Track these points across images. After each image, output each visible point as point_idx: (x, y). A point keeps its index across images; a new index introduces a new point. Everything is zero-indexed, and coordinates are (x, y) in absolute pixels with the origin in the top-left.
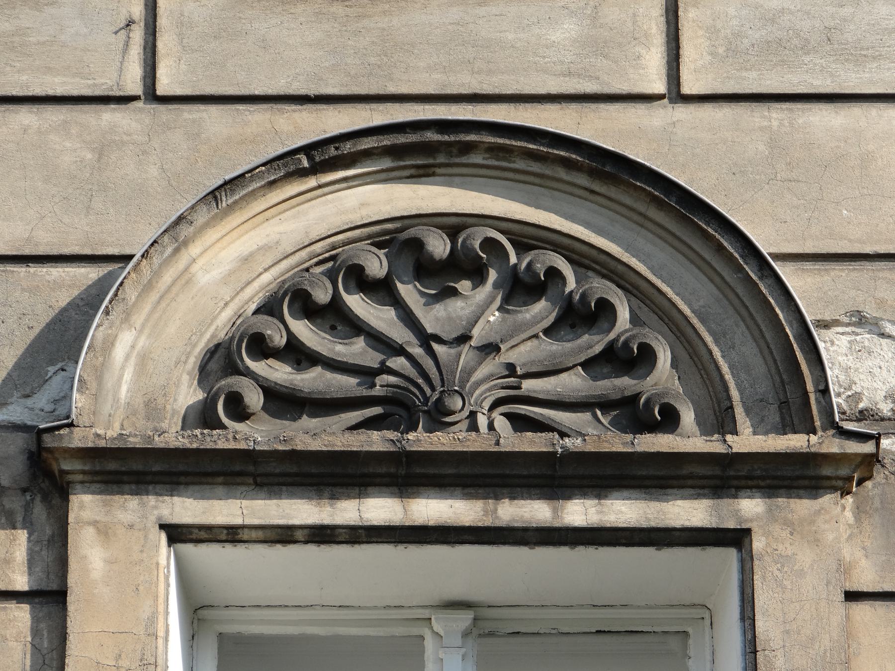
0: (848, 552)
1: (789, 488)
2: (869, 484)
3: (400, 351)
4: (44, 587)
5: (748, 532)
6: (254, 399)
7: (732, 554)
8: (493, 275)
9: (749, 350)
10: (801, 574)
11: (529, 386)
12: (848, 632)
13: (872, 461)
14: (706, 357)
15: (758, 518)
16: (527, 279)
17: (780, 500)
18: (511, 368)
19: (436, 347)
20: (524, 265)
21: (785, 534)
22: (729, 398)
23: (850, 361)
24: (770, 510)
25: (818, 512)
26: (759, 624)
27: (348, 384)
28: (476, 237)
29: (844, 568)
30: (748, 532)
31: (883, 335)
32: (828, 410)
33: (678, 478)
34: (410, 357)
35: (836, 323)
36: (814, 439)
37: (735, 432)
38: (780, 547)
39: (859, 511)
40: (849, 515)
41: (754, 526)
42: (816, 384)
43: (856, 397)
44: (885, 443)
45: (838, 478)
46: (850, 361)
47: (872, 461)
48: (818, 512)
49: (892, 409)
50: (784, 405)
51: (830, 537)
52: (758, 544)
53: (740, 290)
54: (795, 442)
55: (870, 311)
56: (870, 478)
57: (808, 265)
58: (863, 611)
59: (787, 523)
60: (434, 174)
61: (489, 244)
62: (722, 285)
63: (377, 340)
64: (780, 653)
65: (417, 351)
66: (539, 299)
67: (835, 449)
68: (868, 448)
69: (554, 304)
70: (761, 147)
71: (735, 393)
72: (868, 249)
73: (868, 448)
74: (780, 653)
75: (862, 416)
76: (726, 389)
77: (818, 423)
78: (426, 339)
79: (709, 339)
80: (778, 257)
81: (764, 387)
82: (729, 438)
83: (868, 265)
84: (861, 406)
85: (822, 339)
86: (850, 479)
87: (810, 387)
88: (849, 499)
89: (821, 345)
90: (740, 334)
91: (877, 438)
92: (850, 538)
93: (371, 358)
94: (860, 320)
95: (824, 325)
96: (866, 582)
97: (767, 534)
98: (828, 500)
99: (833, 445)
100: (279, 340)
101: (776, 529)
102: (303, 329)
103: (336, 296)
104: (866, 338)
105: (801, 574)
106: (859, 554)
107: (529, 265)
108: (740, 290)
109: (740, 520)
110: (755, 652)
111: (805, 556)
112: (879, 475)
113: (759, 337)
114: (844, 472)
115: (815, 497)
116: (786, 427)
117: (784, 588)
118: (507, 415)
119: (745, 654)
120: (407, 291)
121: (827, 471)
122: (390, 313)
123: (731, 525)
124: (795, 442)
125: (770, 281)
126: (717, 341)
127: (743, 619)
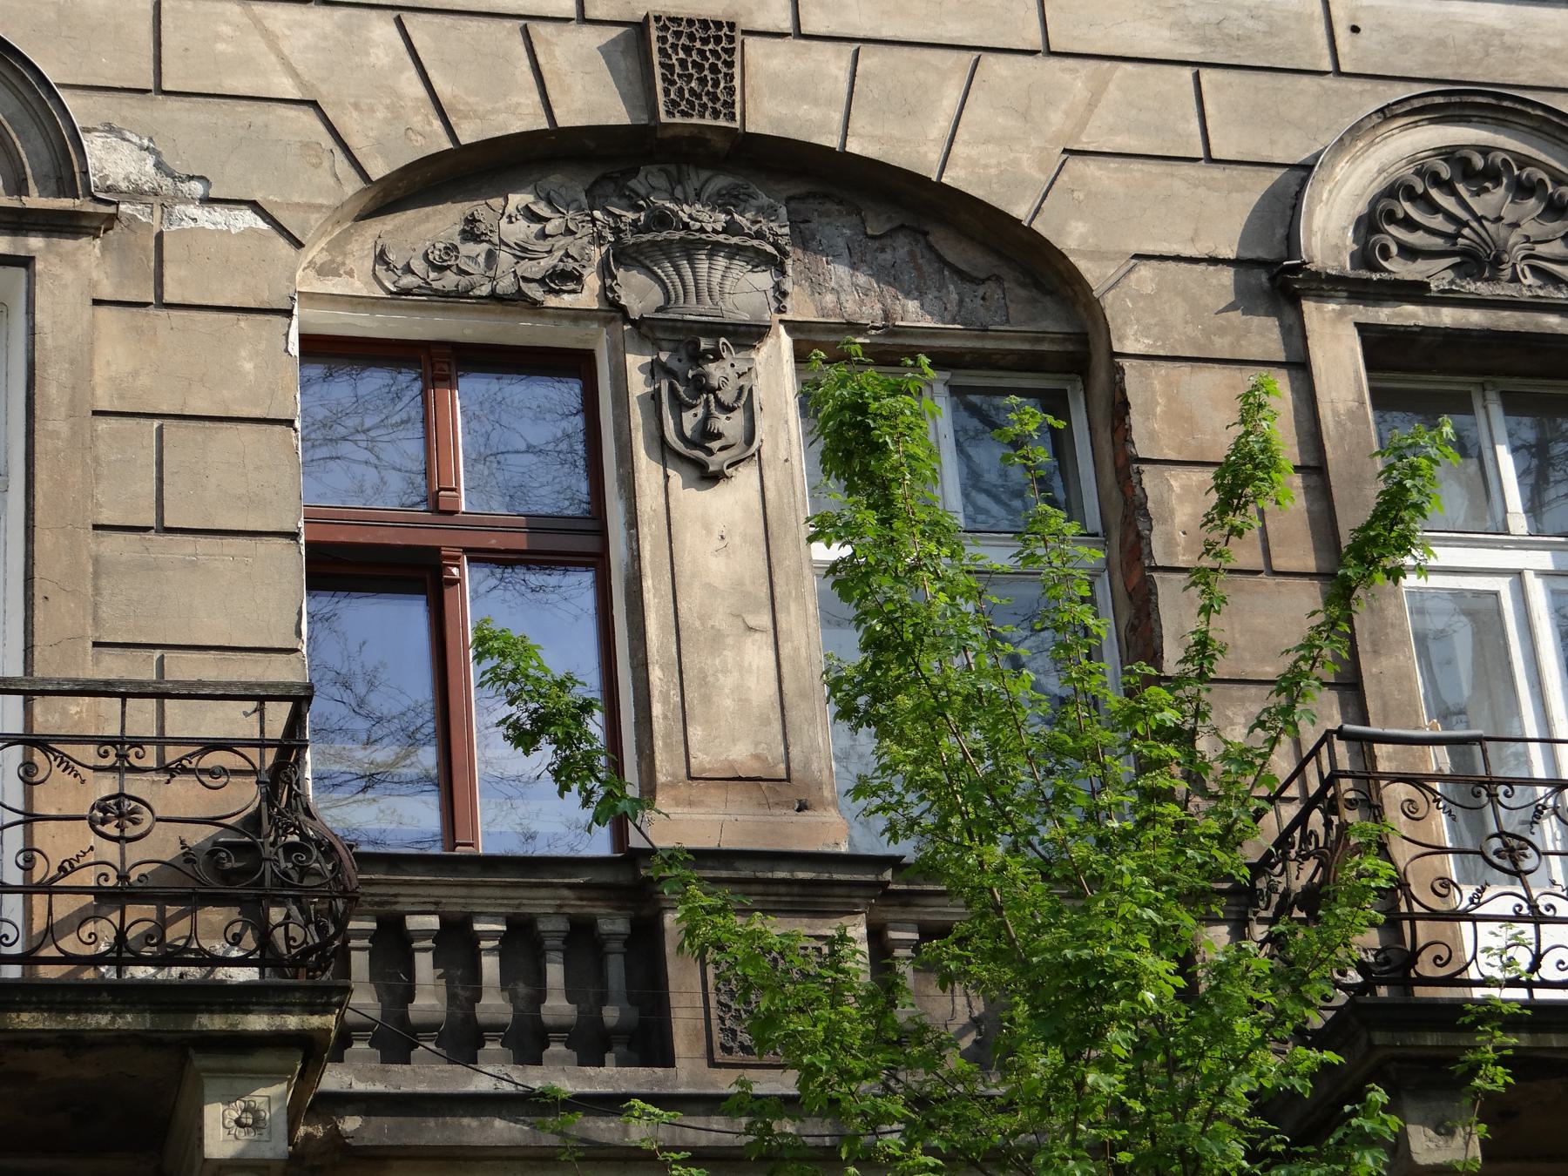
0: (95, 275)
1: (61, 232)
2: (111, 232)
3: (1466, 224)
4: (1292, 359)
5: (33, 258)
6: (1394, 249)
7: (22, 271)
8: (1505, 181)
9: (39, 143)
10: (65, 286)
11: (1541, 249)
12: (93, 325)
13: (113, 219)
14: (11, 146)
15: (39, 250)
16: (1526, 183)
17: (55, 240)
18: (1527, 239)
19: (1485, 223)
20: (1524, 176)
21: (56, 261)
22: (25, 173)
23: (102, 154)
24: (47, 246)
25: (78, 248)
26: (38, 317)
27: (1438, 243)
28: (1499, 157)
29: (93, 285)
30: (33, 258)
31: (124, 139)
32: (87, 185)
33: (70, 226)
34: (1472, 229)
35: (95, 130)
36: (77, 202)
37: (27, 195)
38: (53, 269)
39: (104, 249)
40: (97, 251)
41: (37, 255)
42: (80, 167)
43: (106, 177)
44: (122, 207)
45: (91, 228)
46: (102, 154)
47: (113, 219)
48: (78, 248)
49: (527, 207)
50: (59, 179)
51: (85, 264)
52: (39, 266)
53: (35, 106)
54: (65, 203)
55: (117, 124)
56: (112, 228)
57: (79, 92)
58: (103, 311)
59: (59, 254)
60: (1470, 122)
61: (1505, 161)
62: (25, 103)
63: (1450, 217)
64: (50, 336)
65: (1474, 224)
66: (1530, 197)
67: (91, 210)
68: (111, 210)
69: (1540, 201)
70: (52, 15)
71: (28, 170)
72: (117, 85)
73: (111, 210)
74: (50, 336)
75: (109, 189)
76: (24, 167)
77: (80, 193)
78: (1479, 219)
79: (13, 135)
80: (59, 85)
81: (47, 168)
82: (24, 198)
83: (116, 94)
84: (108, 183)
85: (86, 141)
86: (100, 229)
87: (76, 169)
88: (98, 241)
89: (85, 143)
90: (34, 133)
91: (117, 204)
92: (97, 266)
93: (1450, 228)
94: (110, 129)
95: (87, 130)
96: (106, 293)
97: (45, 260)
98: (84, 241)
99: (90, 207)
100: (1401, 215)
101: (51, 258)
102: (1408, 207)
103: (1426, 189)
104: (113, 140)
105: (65, 286)
106: (102, 276)
107: (1528, 176)
108: (35, 106)
109: (28, 250)
110: (34, 334)
111: (69, 276)
112: (117, 227)
113: (46, 136)
114: (95, 224)
115: (76, 238)
116: (60, 193)
117: (54, 295)
118: (1530, 266)
119: (27, 335)
120: (1461, 188)
121: (85, 223)
122: (1452, 199)
123: (22, 253)
124: (65, 203)
125: (55, 100)
126: (18, 137)
127: (27, 313)
